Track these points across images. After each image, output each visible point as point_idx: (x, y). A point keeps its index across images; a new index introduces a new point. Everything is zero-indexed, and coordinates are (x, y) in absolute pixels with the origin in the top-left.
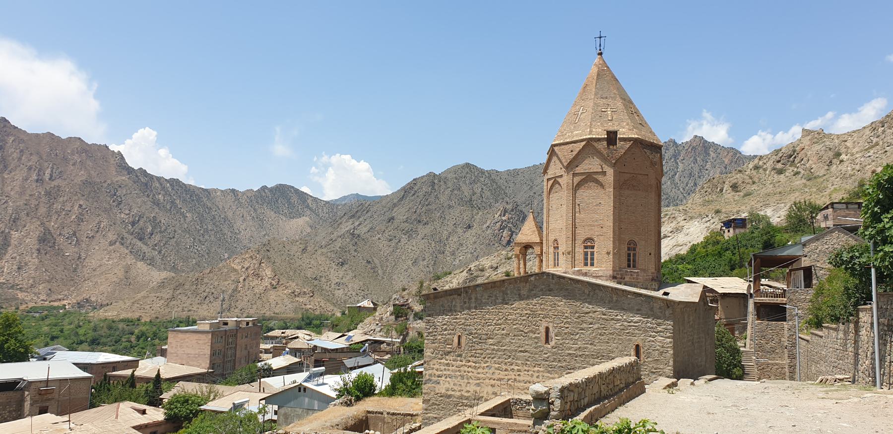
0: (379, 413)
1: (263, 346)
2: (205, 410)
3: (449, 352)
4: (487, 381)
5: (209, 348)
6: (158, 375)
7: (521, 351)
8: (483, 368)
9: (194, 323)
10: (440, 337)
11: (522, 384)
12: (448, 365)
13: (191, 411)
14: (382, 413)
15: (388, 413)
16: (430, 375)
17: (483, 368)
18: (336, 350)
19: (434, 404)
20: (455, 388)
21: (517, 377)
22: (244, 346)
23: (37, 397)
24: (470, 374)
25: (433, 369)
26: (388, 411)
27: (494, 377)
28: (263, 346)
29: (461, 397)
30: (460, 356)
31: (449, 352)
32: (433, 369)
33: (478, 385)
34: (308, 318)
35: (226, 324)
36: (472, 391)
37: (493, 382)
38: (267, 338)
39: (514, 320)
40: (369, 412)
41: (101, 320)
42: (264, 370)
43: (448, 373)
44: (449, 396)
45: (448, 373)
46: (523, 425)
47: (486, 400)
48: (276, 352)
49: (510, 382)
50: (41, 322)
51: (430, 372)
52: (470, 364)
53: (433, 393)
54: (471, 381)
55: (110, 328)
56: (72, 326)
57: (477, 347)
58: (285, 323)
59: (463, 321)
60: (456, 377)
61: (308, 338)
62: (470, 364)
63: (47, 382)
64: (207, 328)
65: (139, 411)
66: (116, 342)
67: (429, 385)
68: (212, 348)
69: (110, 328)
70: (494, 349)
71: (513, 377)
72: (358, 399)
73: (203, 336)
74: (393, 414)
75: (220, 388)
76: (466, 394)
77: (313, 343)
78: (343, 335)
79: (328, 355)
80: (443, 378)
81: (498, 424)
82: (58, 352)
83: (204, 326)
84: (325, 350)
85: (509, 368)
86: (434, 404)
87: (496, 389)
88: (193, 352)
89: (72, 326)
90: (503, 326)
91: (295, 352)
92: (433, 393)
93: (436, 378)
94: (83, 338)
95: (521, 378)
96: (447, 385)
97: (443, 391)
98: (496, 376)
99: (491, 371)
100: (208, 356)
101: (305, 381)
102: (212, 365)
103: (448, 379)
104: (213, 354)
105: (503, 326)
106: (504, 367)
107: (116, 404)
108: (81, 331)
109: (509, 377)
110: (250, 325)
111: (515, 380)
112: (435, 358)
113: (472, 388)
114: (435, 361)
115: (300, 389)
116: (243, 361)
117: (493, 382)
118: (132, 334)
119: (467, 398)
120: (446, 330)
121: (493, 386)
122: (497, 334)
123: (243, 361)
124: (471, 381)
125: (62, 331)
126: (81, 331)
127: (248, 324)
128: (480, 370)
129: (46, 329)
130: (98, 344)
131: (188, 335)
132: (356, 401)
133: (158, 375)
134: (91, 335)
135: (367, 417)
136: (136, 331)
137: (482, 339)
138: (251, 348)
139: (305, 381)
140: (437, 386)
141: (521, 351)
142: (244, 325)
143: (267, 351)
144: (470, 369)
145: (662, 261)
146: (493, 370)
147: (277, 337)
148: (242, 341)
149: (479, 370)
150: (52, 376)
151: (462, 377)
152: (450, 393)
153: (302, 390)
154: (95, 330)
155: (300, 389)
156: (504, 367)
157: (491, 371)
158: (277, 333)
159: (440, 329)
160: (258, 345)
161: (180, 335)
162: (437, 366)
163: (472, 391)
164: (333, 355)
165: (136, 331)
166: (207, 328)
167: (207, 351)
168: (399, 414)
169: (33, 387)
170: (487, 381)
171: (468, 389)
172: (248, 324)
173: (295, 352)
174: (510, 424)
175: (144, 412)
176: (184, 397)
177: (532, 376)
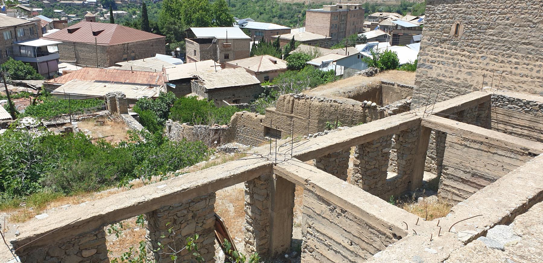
0: (391, 84)
1: (367, 23)
2: (310, 64)
3: (445, 41)
4: (479, 71)
5: (329, 23)
6: (293, 39)
7: (524, 43)
8: (478, 58)
9: (321, 6)
10: (437, 25)
11: (518, 77)
12: (442, 52)
13: (301, 64)
14: (394, 85)
15: (398, 85)
16: (425, 60)
17: (478, 58)
18: (409, 29)
19: (424, 86)
20: (446, 74)
21: (514, 71)
22: (352, 23)
23: (223, 48)
24: (462, 63)
25: (427, 55)
26: (399, 83)
27: (487, 68)
28: (367, 23)
29: (450, 83)
30: (455, 44)
31: (445, 41)
32: (427, 55)
33: (469, 74)
34: (405, 5)
35: (341, 7)
36: (462, 78)
37: (485, 72)
38: (371, 18)
39: (523, 9)
40: (383, 83)
41: (284, 4)
42: (361, 39)
43: (442, 60)
44: (440, 81)
45: (442, 60)
46: (481, 136)
47: (476, 89)
48: (372, 27)
49: (504, 74)
50: (255, 4)
51: (425, 57)
52: (464, 53)
53: (424, 76)
54: (462, 69)
55: (288, 9)
56: (270, 7)
57: (475, 36)
58: (390, 8)
59: (464, 9)
60: (448, 64)
61: (395, 18)
62: (464, 53)
63: (227, 40)
64: (329, 10)
65: (272, 61)
66: (292, 17)
67: (422, 69)
68: (331, 23)
69: (288, 9)
70: (492, 40)
71: (509, 69)
72: (382, 70)
73: (326, 15)
74: (403, 86)
75: (322, 50)
76: (456, 81)
77: (396, 23)
78: (417, 18)
79: (402, 31)
80: (436, 64)
81: (451, 129)
82: (249, 22)
83: (327, 8)
84: (403, 28)
85: (506, 60)
86: (424, 86)
87: (486, 80)
88: (320, 25)
89: (270, 7)
90: (509, 15)
91: (384, 28)
92: (424, 76)
93: (430, 64)
94: (275, 14)
95: (518, 71)
96: (439, 71)
97: (434, 76)
98: (490, 67)
99: (485, 62)
100: (328, 28)
101: (363, 51)
102: (331, 34)
103: (441, 65)
104: (331, 28)
105: (509, 15)
106: (501, 59)
107: (261, 57)
108: (274, 10)
109: (505, 69)
110: (357, 8)
111: (511, 72)
112: (430, 45)
113: (462, 76)
114: (430, 48)
115: (359, 56)
116: (351, 32)
117: (485, 72)
118: (300, 12)
119: (456, 85)
120: (445, 18)
121: (484, 76)
122: (499, 24)
123: (351, 32)
124: (462, 69)
125: (265, 10)
126: (274, 10)
127: (356, 8)
128: (474, 60)
129: (257, 8)
130: (283, 18)
131: (317, 14)
132: (380, 72)
133: (293, 39)
134: (279, 12)
135: (381, 87)
136: (302, 11)
137: (480, 29)
138: (357, 23)
139: (363, 51)
140: (430, 71)
141: (524, 43)
142: (353, 9)
143: (369, 26)
144: (463, 58)
145: (388, 178)
146: (487, 60)
147: (377, 17)
148: (351, 19)
149: (473, 60)
150: (229, 37)
151: (455, 65)
152: (440, 78)
153: (360, 57)
154: (281, 10)
155: (359, 56)
156: (501, 59)
157: (485, 62)
158: (377, 14)
159: (439, 17)
160: (362, 22)
161: (313, 14)
162: (431, 53)
163: (462, 78)
164: (406, 32)
165: (302, 11)
166: (329, 10)
167: (328, 25)
168: (407, 87)
169: (220, 42)
170: (479, 71)
171: (458, 76)
172: (356, 8)
173: (384, 28)
174: (465, 132)
175: (275, 62)
176: (298, 55)
177: (532, 70)
